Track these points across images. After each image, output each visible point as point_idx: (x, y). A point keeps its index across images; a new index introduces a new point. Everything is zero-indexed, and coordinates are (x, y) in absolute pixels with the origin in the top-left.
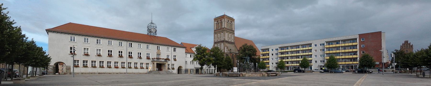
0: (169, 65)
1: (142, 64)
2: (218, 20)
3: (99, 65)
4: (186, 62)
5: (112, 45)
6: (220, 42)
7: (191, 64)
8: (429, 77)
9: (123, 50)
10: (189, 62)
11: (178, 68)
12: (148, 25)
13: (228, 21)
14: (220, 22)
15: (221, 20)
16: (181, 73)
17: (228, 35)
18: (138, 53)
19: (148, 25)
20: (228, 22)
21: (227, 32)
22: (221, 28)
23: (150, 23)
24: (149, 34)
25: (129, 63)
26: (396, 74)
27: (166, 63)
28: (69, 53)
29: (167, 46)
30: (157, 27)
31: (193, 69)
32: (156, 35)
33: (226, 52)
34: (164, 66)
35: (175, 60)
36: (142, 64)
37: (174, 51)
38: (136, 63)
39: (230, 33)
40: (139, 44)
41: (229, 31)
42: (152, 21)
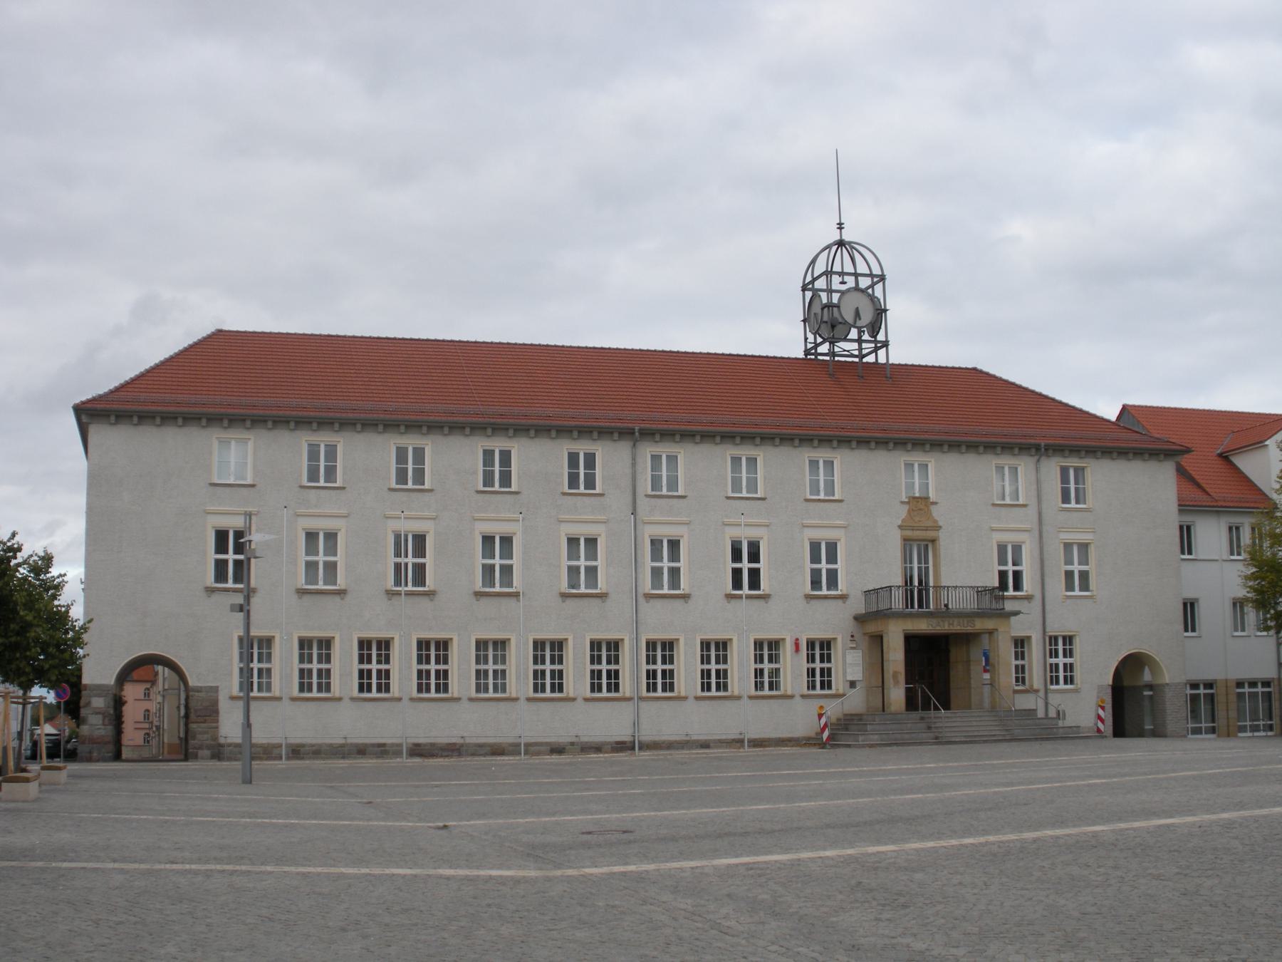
0: (1021, 644)
1: (768, 649)
3: (356, 675)
4: (1189, 608)
7: (1239, 624)
8: (835, 309)
10: (1214, 614)
11: (1118, 675)
12: (813, 262)
16: (1158, 733)
18: (397, 537)
19: (813, 262)
23: (829, 247)
24: (824, 348)
25: (651, 645)
27: (991, 633)
28: (563, 590)
29: (728, 438)
30: (882, 278)
31: (1266, 684)
32: (882, 353)
34: (976, 654)
35: (1079, 581)
36: (768, 649)
37: (1066, 499)
38: (716, 649)
42: (840, 226)
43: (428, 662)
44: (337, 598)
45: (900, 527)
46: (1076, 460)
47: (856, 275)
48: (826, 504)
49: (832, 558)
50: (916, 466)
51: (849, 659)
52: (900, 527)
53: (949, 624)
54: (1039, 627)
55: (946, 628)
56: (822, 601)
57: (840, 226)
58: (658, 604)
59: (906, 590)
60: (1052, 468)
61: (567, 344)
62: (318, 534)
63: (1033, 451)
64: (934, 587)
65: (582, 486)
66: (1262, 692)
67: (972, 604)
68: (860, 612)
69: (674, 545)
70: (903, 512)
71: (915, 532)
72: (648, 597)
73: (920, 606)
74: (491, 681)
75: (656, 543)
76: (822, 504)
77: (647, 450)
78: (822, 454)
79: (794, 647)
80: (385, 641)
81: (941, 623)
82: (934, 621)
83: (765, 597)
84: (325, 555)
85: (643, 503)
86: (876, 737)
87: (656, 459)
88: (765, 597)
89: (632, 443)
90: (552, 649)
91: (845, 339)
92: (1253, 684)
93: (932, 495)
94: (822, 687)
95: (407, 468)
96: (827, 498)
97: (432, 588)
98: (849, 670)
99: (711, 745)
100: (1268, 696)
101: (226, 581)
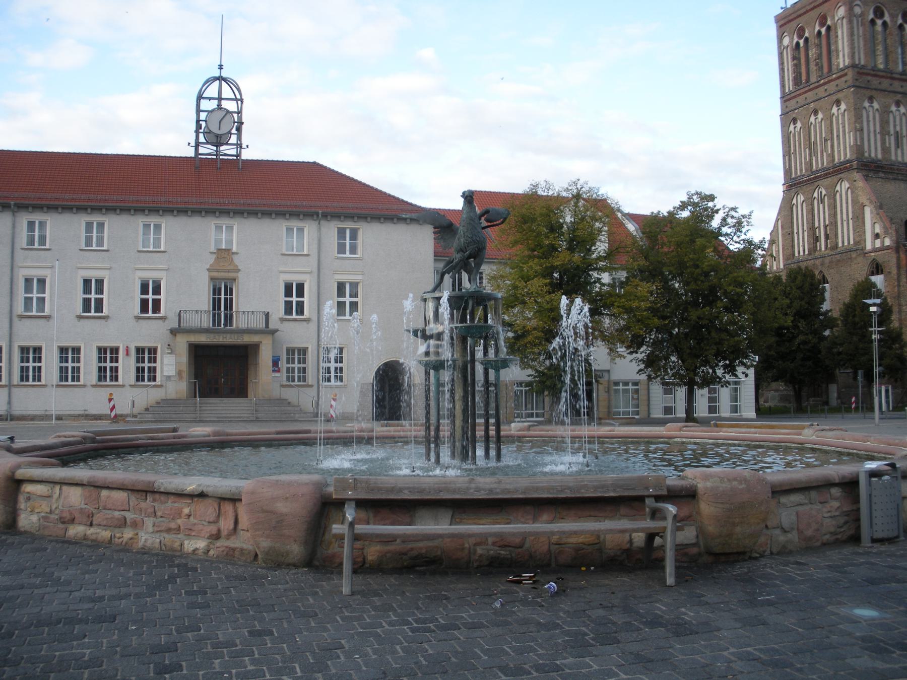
1: (108, 354)
2: (801, 22)
5: (105, 248)
6: (826, 176)
9: (110, 269)
13: (879, 13)
14: (819, 33)
15: (823, 21)
17: (885, 112)
20: (873, 22)
21: (868, 93)
22: (825, 70)
25: (24, 350)
26: (855, 416)
28: (281, 316)
33: (869, 247)
36: (108, 354)
39: (899, 97)
40: (147, 226)
41: (886, 83)
42: (221, 67)
43: (143, 362)
44: (305, 323)
45: (208, 270)
46: (350, 223)
47: (220, 99)
48: (153, 254)
49: (100, 290)
50: (224, 227)
51: (166, 361)
52: (208, 270)
53: (223, 338)
54: (315, 341)
55: (221, 340)
56: (147, 321)
57: (221, 67)
58: (27, 322)
59: (214, 315)
60: (330, 230)
61: (99, 152)
62: (33, 279)
63: (315, 217)
64: (236, 311)
65: (348, 252)
66: (632, 389)
67: (243, 323)
68: (175, 327)
69: (42, 282)
70: (212, 259)
71: (219, 273)
72: (21, 317)
73: (225, 325)
74: (146, 374)
75: (28, 281)
76: (150, 254)
77: (24, 219)
78: (153, 220)
79: (125, 353)
80: (27, 348)
81: (217, 337)
82: (212, 335)
83: (106, 318)
84: (96, 293)
85: (19, 254)
86: (150, 415)
87: (31, 225)
88: (106, 318)
89: (317, 222)
90: (299, 354)
91: (227, 144)
92: (626, 384)
93: (234, 249)
94: (111, 380)
95: (350, 240)
96: (154, 250)
97: (308, 317)
98: (165, 369)
99: (63, 418)
100: (637, 391)
101: (147, 312)
